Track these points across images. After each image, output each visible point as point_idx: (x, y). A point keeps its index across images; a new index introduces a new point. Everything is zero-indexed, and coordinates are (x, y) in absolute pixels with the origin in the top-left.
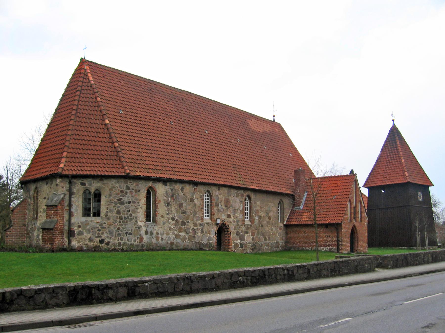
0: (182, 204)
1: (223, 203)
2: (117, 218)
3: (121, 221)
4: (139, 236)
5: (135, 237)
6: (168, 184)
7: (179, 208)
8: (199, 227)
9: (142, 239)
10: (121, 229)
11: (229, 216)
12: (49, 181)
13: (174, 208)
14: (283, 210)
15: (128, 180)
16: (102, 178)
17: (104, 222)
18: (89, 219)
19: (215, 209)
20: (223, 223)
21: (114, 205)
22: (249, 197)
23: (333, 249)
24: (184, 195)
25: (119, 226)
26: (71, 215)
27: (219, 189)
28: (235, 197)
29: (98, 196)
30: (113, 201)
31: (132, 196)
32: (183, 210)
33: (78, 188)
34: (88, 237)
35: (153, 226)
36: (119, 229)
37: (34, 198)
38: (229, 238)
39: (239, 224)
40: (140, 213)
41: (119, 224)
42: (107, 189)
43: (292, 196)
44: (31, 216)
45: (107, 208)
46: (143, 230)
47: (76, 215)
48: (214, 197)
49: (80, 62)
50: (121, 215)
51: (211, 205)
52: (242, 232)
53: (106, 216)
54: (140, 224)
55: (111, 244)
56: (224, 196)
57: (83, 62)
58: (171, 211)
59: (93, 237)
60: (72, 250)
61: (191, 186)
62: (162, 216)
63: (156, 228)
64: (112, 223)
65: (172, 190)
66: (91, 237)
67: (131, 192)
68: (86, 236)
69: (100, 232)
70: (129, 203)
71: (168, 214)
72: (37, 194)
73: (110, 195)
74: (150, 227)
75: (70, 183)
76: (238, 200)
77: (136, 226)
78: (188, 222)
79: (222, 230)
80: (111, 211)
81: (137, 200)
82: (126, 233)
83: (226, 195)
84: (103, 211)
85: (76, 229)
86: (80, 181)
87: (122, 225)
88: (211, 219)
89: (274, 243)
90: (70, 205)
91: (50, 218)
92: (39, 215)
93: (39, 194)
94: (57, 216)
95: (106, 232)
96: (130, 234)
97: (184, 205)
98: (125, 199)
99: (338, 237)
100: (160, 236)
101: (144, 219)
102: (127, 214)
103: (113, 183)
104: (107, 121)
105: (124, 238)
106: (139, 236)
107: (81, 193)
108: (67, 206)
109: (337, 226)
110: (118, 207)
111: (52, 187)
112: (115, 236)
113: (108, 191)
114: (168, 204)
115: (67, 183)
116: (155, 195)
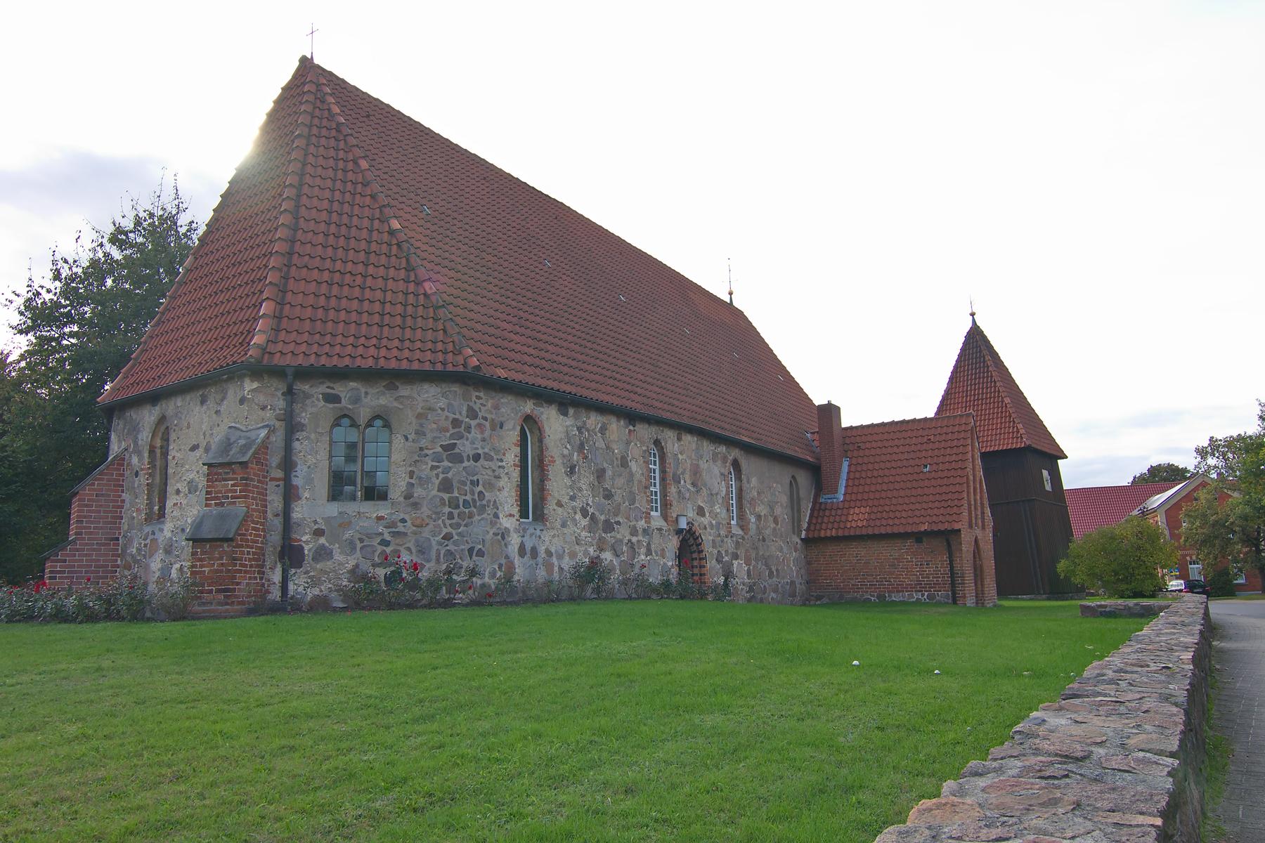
0: (604, 470)
1: (687, 476)
2: (444, 504)
3: (456, 512)
4: (503, 561)
5: (493, 563)
8: (640, 538)
9: (511, 568)
10: (456, 537)
12: (212, 392)
13: (585, 480)
15: (471, 389)
18: (351, 508)
19: (673, 490)
21: (430, 463)
22: (736, 464)
23: (941, 595)
24: (608, 448)
25: (450, 530)
26: (290, 495)
31: (484, 440)
33: (314, 406)
35: (538, 532)
36: (448, 537)
37: (152, 451)
39: (722, 533)
40: (505, 493)
43: (815, 470)
44: (138, 510)
45: (411, 474)
47: (307, 495)
48: (669, 460)
49: (298, 69)
51: (663, 479)
53: (408, 496)
56: (690, 458)
57: (307, 67)
58: (580, 490)
60: (287, 606)
62: (559, 504)
63: (546, 537)
64: (427, 521)
65: (579, 429)
66: (357, 566)
68: (341, 564)
69: (388, 550)
70: (477, 458)
71: (573, 498)
72: (166, 439)
73: (420, 433)
74: (531, 535)
75: (290, 392)
77: (494, 530)
78: (618, 523)
79: (689, 544)
80: (423, 482)
81: (497, 452)
82: (471, 550)
86: (323, 389)
87: (459, 525)
88: (665, 517)
90: (288, 465)
91: (222, 504)
92: (169, 504)
93: (173, 436)
94: (245, 497)
95: (409, 549)
96: (481, 554)
97: (609, 473)
100: (554, 560)
102: (473, 493)
103: (429, 394)
104: (396, 224)
106: (503, 561)
107: (325, 425)
108: (279, 467)
109: (949, 537)
111: (223, 408)
113: (414, 421)
114: (571, 470)
115: (279, 394)
116: (541, 441)
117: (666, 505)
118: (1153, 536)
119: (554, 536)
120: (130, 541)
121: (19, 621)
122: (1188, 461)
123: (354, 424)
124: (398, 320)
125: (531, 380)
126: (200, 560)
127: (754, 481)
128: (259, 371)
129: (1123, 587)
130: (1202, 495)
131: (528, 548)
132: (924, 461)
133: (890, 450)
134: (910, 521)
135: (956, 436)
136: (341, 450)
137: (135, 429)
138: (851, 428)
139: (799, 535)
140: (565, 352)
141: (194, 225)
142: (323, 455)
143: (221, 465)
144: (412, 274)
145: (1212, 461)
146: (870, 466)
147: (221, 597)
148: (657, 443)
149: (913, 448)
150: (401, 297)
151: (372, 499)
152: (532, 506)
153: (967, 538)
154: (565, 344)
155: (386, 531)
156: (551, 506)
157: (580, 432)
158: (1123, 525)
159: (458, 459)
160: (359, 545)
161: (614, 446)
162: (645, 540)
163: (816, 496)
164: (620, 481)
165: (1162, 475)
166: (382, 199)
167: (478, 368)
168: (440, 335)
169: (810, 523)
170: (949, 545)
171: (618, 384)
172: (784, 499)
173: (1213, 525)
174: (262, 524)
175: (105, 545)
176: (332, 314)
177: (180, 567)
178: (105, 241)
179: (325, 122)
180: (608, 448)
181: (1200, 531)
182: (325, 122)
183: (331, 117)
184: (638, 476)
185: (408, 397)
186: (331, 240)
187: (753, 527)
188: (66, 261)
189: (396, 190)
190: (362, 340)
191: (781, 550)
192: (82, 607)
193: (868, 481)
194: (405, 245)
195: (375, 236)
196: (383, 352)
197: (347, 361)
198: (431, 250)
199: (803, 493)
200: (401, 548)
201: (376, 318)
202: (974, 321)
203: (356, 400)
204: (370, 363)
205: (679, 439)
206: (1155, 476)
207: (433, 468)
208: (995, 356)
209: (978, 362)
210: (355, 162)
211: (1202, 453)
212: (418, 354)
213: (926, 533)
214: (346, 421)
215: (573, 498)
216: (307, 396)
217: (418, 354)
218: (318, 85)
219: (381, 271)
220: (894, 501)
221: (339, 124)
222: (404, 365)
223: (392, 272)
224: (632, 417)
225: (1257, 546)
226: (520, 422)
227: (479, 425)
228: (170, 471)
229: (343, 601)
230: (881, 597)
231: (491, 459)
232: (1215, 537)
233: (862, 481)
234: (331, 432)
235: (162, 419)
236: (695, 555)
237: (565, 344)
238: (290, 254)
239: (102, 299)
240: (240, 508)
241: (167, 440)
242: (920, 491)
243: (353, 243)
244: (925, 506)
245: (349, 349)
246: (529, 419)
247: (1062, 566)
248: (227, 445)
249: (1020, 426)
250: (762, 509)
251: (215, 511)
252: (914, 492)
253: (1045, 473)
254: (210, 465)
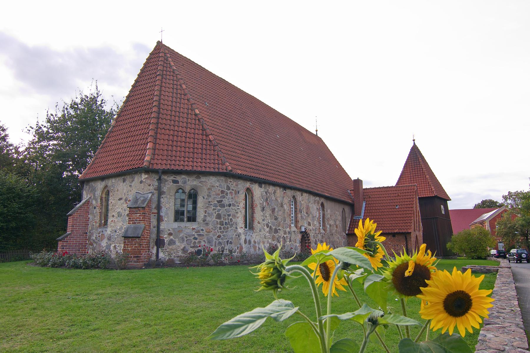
0: (274, 209)
1: (304, 210)
2: (218, 224)
4: (239, 246)
9: (241, 248)
12: (128, 178)
13: (268, 213)
14: (345, 219)
16: (199, 174)
17: (202, 228)
18: (183, 225)
19: (299, 215)
21: (213, 208)
22: (322, 205)
24: (276, 200)
25: (220, 234)
26: (159, 219)
29: (193, 196)
30: (212, 203)
31: (232, 198)
32: (275, 216)
33: (169, 185)
34: (182, 247)
36: (219, 237)
40: (240, 219)
41: (219, 231)
43: (352, 206)
45: (206, 212)
47: (166, 219)
48: (298, 204)
49: (156, 46)
50: (222, 220)
51: (296, 212)
53: (204, 221)
58: (266, 217)
60: (158, 264)
62: (259, 223)
63: (254, 235)
64: (211, 230)
65: (266, 193)
66: (185, 247)
69: (197, 241)
70: (230, 205)
71: (263, 220)
73: (209, 196)
75: (160, 179)
77: (236, 234)
78: (280, 229)
81: (237, 203)
82: (228, 242)
84: (200, 214)
85: (166, 238)
86: (172, 178)
87: (223, 232)
90: (159, 207)
92: (109, 221)
93: (111, 194)
94: (144, 220)
95: (204, 241)
96: (231, 243)
97: (276, 210)
100: (257, 245)
103: (212, 180)
104: (197, 112)
107: (173, 192)
108: (155, 208)
110: (219, 210)
114: (263, 209)
116: (252, 198)
117: (297, 222)
118: (486, 235)
120: (92, 234)
121: (57, 267)
122: (501, 201)
123: (184, 192)
124: (200, 151)
125: (249, 174)
126: (128, 245)
127: (329, 211)
128: (147, 171)
129: (474, 254)
130: (505, 215)
131: (248, 241)
132: (396, 204)
133: (382, 199)
134: (391, 228)
135: (409, 194)
136: (179, 202)
137: (94, 190)
138: (366, 189)
139: (345, 232)
140: (260, 161)
141: (104, 101)
142: (172, 204)
143: (135, 208)
144: (204, 132)
145: (509, 201)
146: (374, 205)
147: (135, 259)
148: (294, 197)
149: (392, 198)
150: (200, 142)
151: (191, 221)
152: (249, 224)
153: (413, 235)
154: (260, 158)
155: (196, 234)
156: (256, 223)
157: (266, 194)
158: (473, 229)
159: (223, 206)
160: (186, 239)
162: (289, 236)
163: (352, 217)
164: (280, 213)
165: (488, 205)
166: (192, 101)
167: (231, 171)
168: (216, 157)
169: (349, 227)
170: (406, 239)
171: (280, 174)
172: (340, 218)
173: (509, 228)
174: (149, 231)
175: (82, 235)
176: (174, 148)
177: (120, 248)
178: (68, 108)
179: (168, 69)
180: (276, 200)
181: (503, 230)
182: (168, 69)
183: (170, 67)
184: (287, 211)
185: (205, 182)
186: (173, 117)
187: (328, 229)
188: (52, 115)
189: (196, 96)
190: (187, 159)
191: (338, 238)
192: (85, 263)
193: (373, 211)
194: (201, 120)
195: (190, 116)
196: (195, 164)
197: (182, 167)
198: (210, 121)
199: (347, 215)
200: (202, 241)
201: (192, 150)
202: (414, 143)
203: (185, 183)
204: (190, 168)
205: (302, 195)
206: (484, 204)
207: (214, 209)
208: (421, 154)
209: (416, 161)
210: (181, 86)
211: (505, 198)
212: (208, 165)
213: (397, 233)
214: (180, 191)
215: (263, 220)
216: (166, 181)
217: (208, 165)
218: (165, 53)
219: (193, 131)
220: (384, 220)
221: (174, 70)
222: (203, 169)
223: (197, 131)
224: (285, 187)
225: (527, 237)
226: (245, 191)
227: (231, 192)
228: (110, 207)
229: (180, 261)
231: (235, 206)
232: (509, 234)
233: (371, 211)
234: (175, 195)
235: (106, 186)
236: (307, 241)
237: (260, 158)
238: (157, 123)
239: (66, 130)
240: (142, 225)
241: (108, 195)
242: (394, 216)
243: (181, 119)
244: (396, 222)
245: (182, 163)
246: (248, 190)
247: (448, 245)
248: (136, 200)
249: (433, 187)
250: (331, 222)
251: (133, 225)
252: (392, 216)
253: (442, 206)
254: (130, 208)
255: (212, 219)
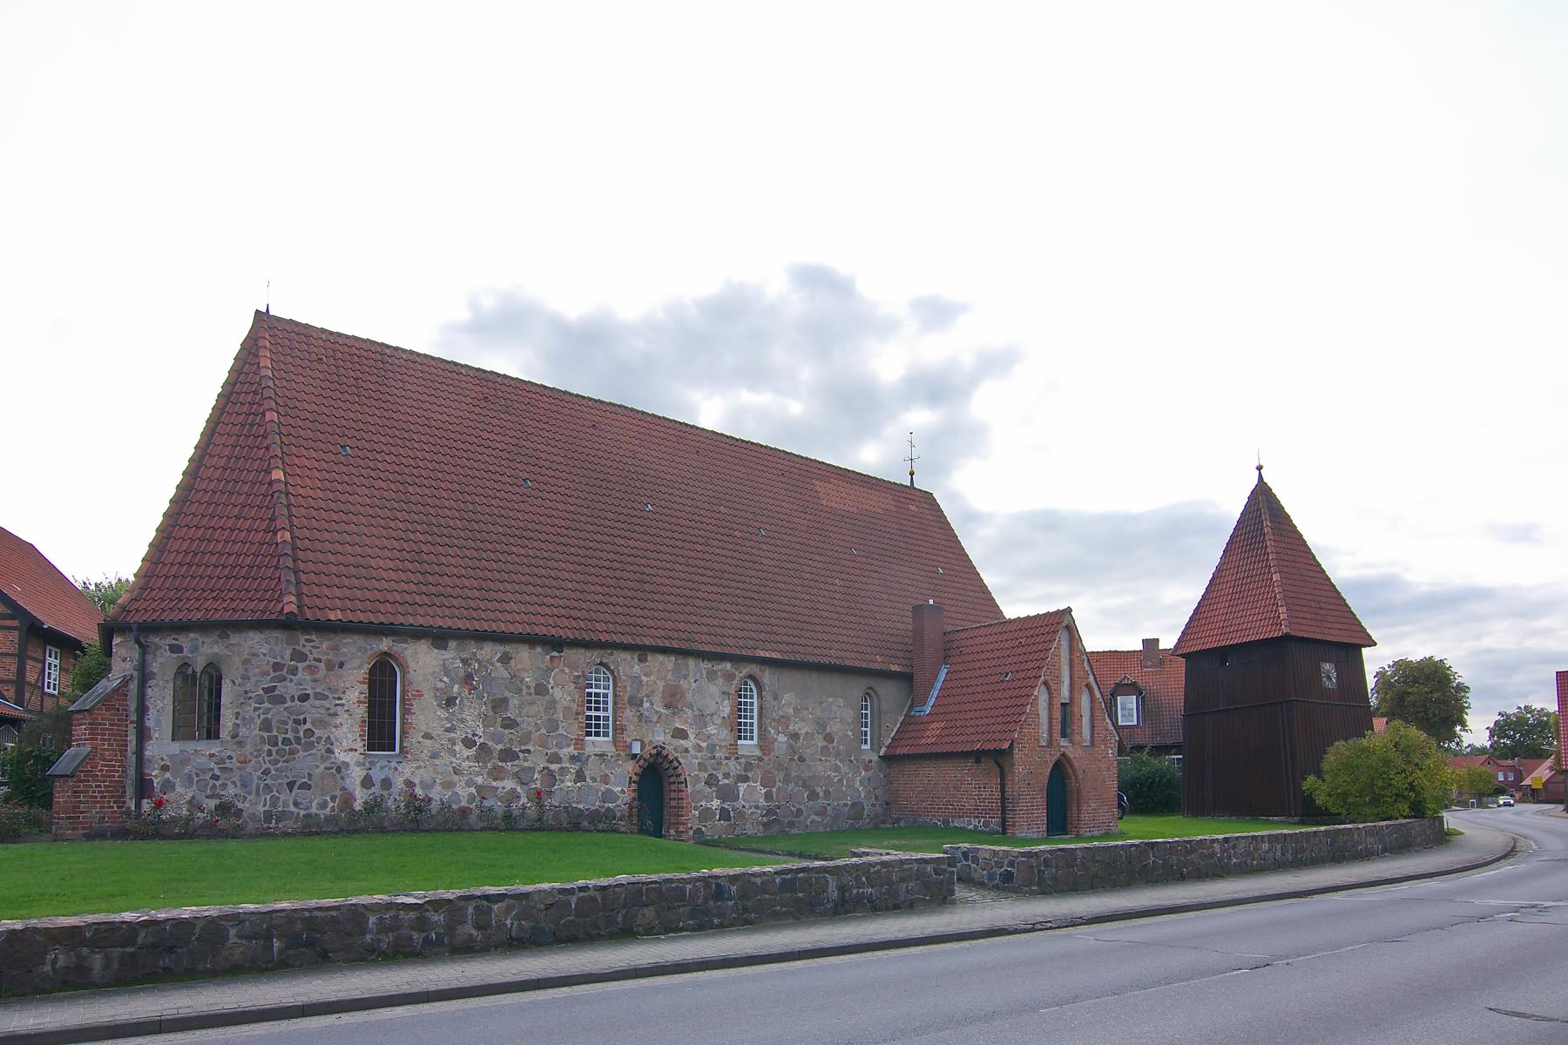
0: (505, 700)
1: (657, 699)
4: (338, 793)
6: (452, 644)
7: (491, 713)
11: (680, 734)
18: (191, 746)
20: (659, 754)
23: (995, 823)
26: (143, 735)
27: (642, 660)
28: (704, 682)
29: (214, 676)
36: (266, 772)
38: (683, 795)
40: (345, 728)
42: (236, 659)
43: (906, 678)
46: (357, 774)
52: (727, 776)
54: (341, 756)
55: (245, 815)
58: (462, 721)
59: (201, 797)
61: (539, 649)
63: (406, 770)
65: (465, 662)
67: (311, 669)
70: (304, 698)
73: (246, 678)
75: (144, 649)
76: (714, 689)
77: (327, 764)
78: (528, 751)
79: (656, 776)
80: (248, 722)
83: (670, 676)
85: (156, 775)
86: (169, 640)
89: (846, 805)
90: (142, 710)
97: (514, 702)
98: (290, 688)
99: (1003, 791)
101: (359, 745)
103: (255, 642)
104: (278, 475)
105: (282, 797)
107: (170, 674)
109: (999, 758)
110: (267, 711)
112: (258, 793)
119: (419, 768)
132: (1007, 669)
161: (524, 675)
203: (195, 649)
205: (641, 660)
207: (256, 709)
209: (1264, 523)
230: (946, 822)
255: (253, 732)
